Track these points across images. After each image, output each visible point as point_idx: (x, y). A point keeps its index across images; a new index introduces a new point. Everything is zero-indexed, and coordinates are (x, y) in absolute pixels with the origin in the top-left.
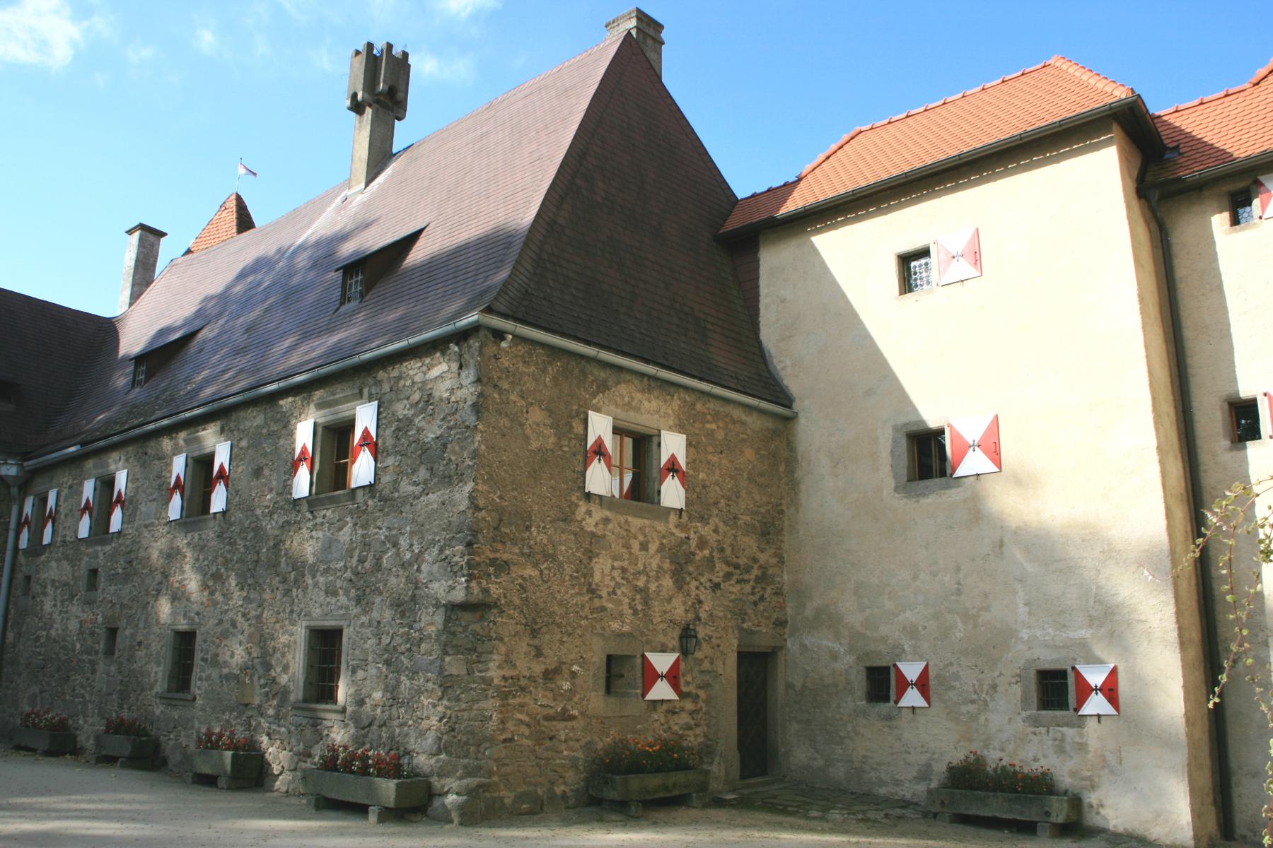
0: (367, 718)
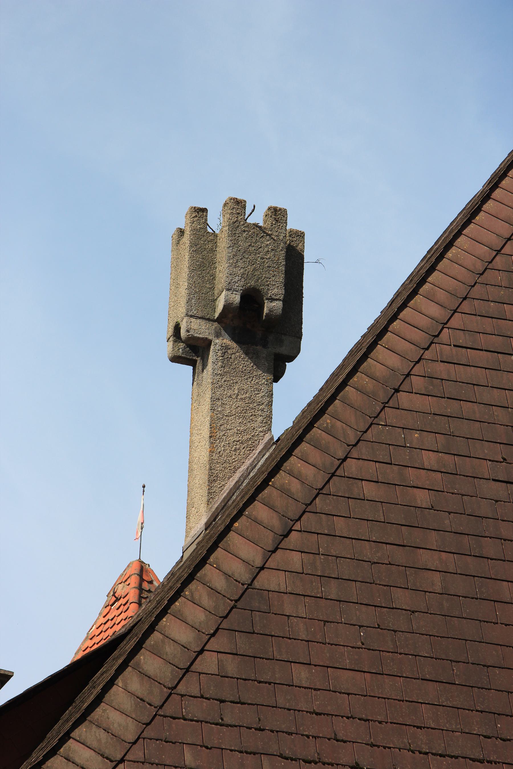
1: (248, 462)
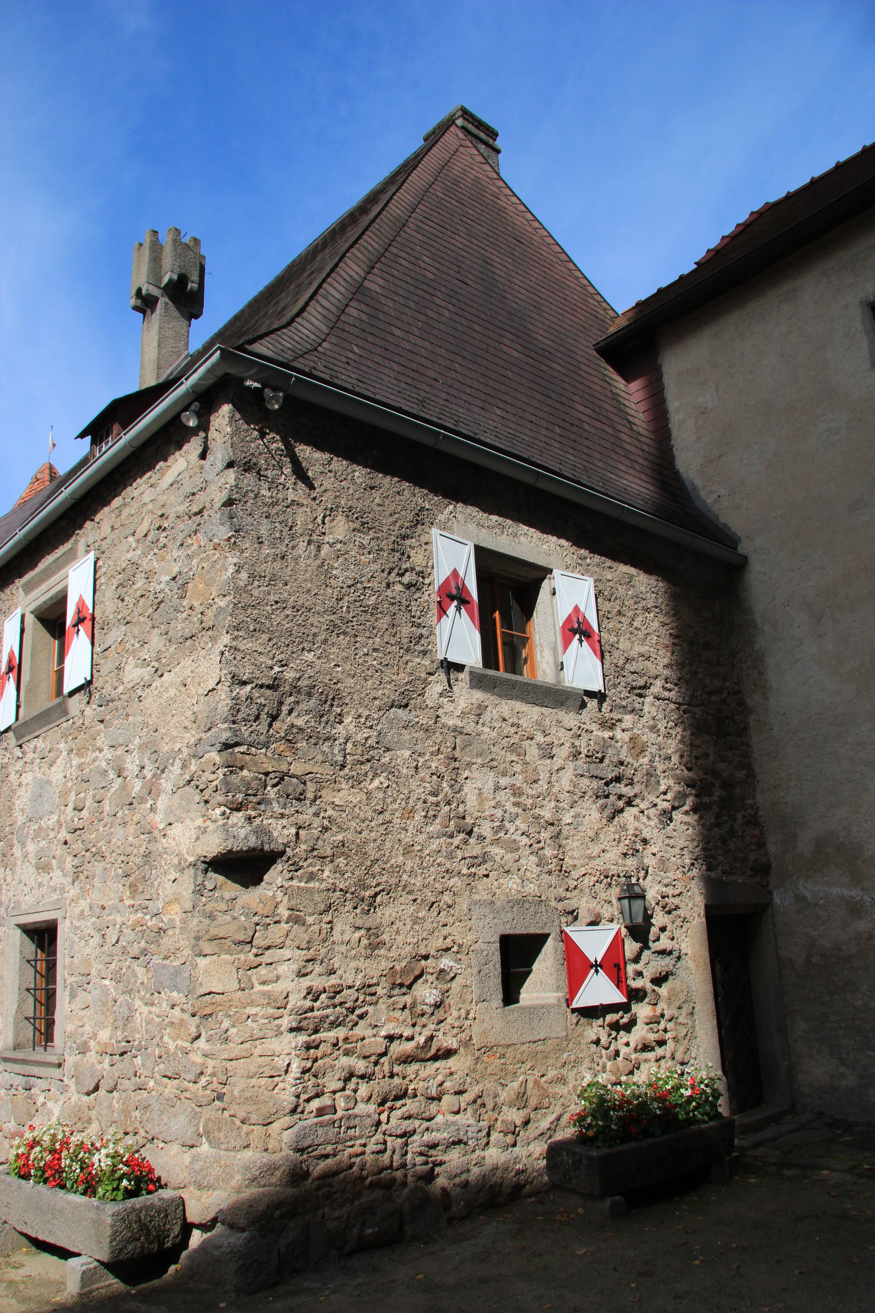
0: (92, 1076)
1: (177, 363)
